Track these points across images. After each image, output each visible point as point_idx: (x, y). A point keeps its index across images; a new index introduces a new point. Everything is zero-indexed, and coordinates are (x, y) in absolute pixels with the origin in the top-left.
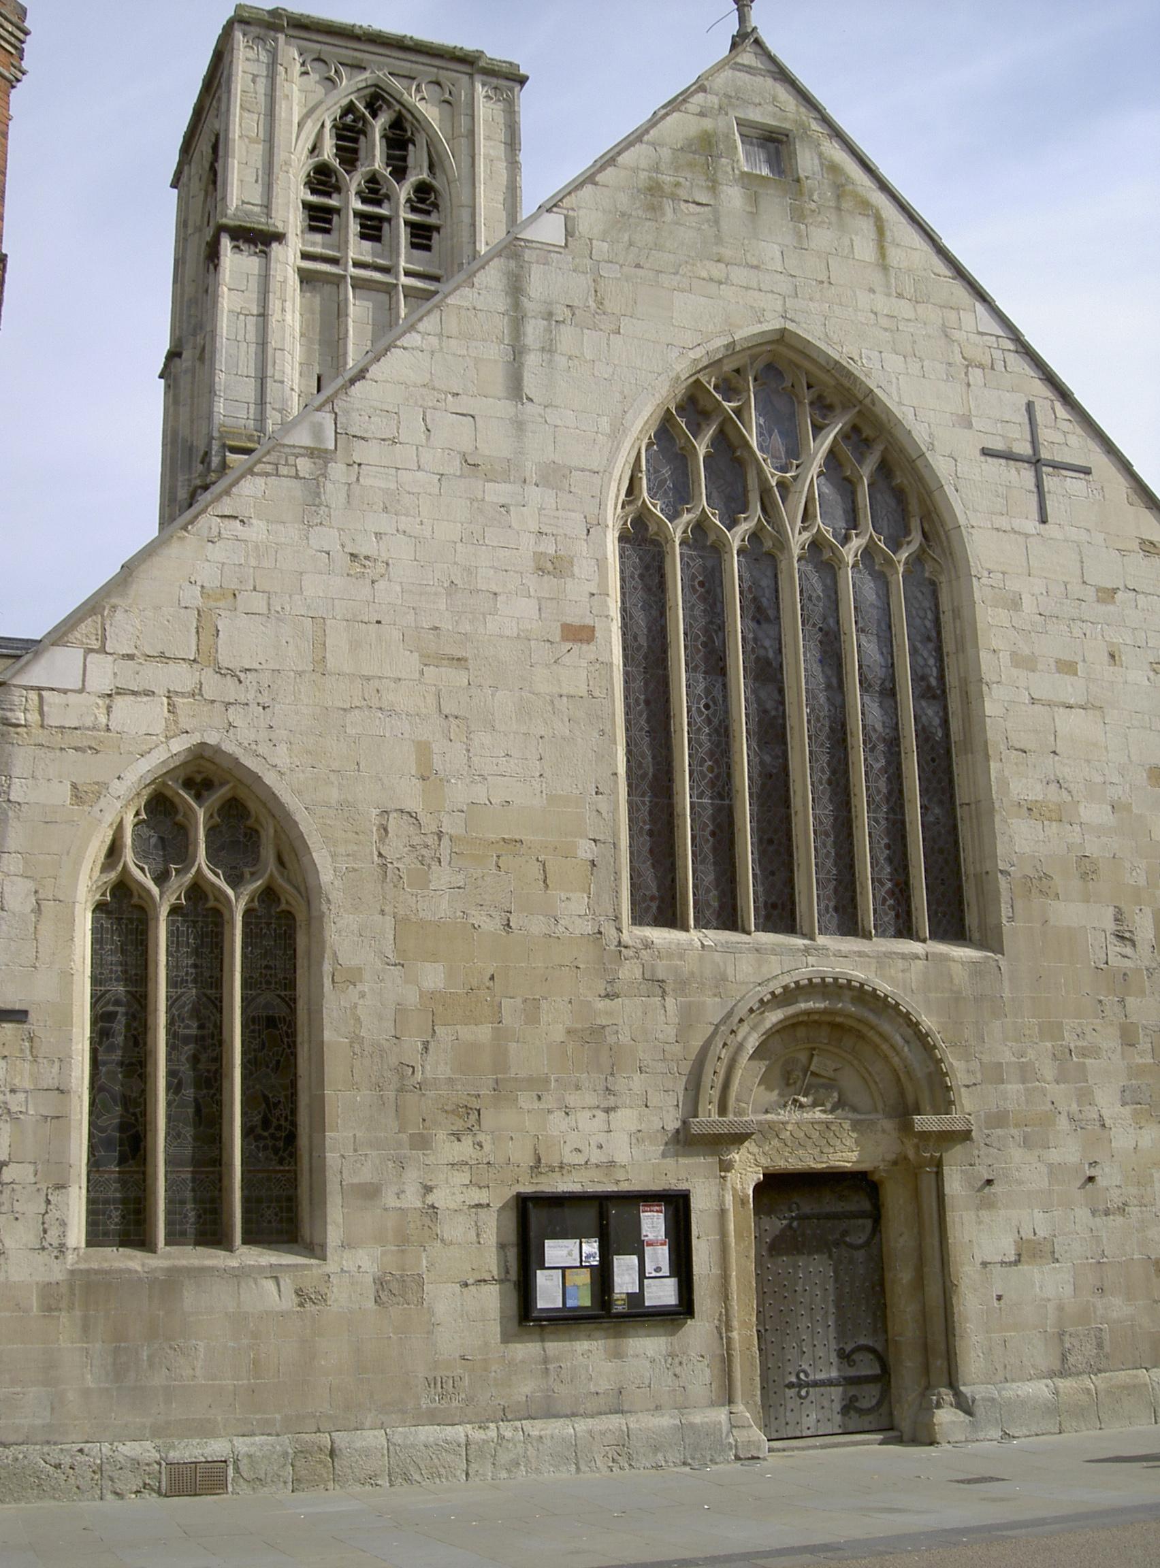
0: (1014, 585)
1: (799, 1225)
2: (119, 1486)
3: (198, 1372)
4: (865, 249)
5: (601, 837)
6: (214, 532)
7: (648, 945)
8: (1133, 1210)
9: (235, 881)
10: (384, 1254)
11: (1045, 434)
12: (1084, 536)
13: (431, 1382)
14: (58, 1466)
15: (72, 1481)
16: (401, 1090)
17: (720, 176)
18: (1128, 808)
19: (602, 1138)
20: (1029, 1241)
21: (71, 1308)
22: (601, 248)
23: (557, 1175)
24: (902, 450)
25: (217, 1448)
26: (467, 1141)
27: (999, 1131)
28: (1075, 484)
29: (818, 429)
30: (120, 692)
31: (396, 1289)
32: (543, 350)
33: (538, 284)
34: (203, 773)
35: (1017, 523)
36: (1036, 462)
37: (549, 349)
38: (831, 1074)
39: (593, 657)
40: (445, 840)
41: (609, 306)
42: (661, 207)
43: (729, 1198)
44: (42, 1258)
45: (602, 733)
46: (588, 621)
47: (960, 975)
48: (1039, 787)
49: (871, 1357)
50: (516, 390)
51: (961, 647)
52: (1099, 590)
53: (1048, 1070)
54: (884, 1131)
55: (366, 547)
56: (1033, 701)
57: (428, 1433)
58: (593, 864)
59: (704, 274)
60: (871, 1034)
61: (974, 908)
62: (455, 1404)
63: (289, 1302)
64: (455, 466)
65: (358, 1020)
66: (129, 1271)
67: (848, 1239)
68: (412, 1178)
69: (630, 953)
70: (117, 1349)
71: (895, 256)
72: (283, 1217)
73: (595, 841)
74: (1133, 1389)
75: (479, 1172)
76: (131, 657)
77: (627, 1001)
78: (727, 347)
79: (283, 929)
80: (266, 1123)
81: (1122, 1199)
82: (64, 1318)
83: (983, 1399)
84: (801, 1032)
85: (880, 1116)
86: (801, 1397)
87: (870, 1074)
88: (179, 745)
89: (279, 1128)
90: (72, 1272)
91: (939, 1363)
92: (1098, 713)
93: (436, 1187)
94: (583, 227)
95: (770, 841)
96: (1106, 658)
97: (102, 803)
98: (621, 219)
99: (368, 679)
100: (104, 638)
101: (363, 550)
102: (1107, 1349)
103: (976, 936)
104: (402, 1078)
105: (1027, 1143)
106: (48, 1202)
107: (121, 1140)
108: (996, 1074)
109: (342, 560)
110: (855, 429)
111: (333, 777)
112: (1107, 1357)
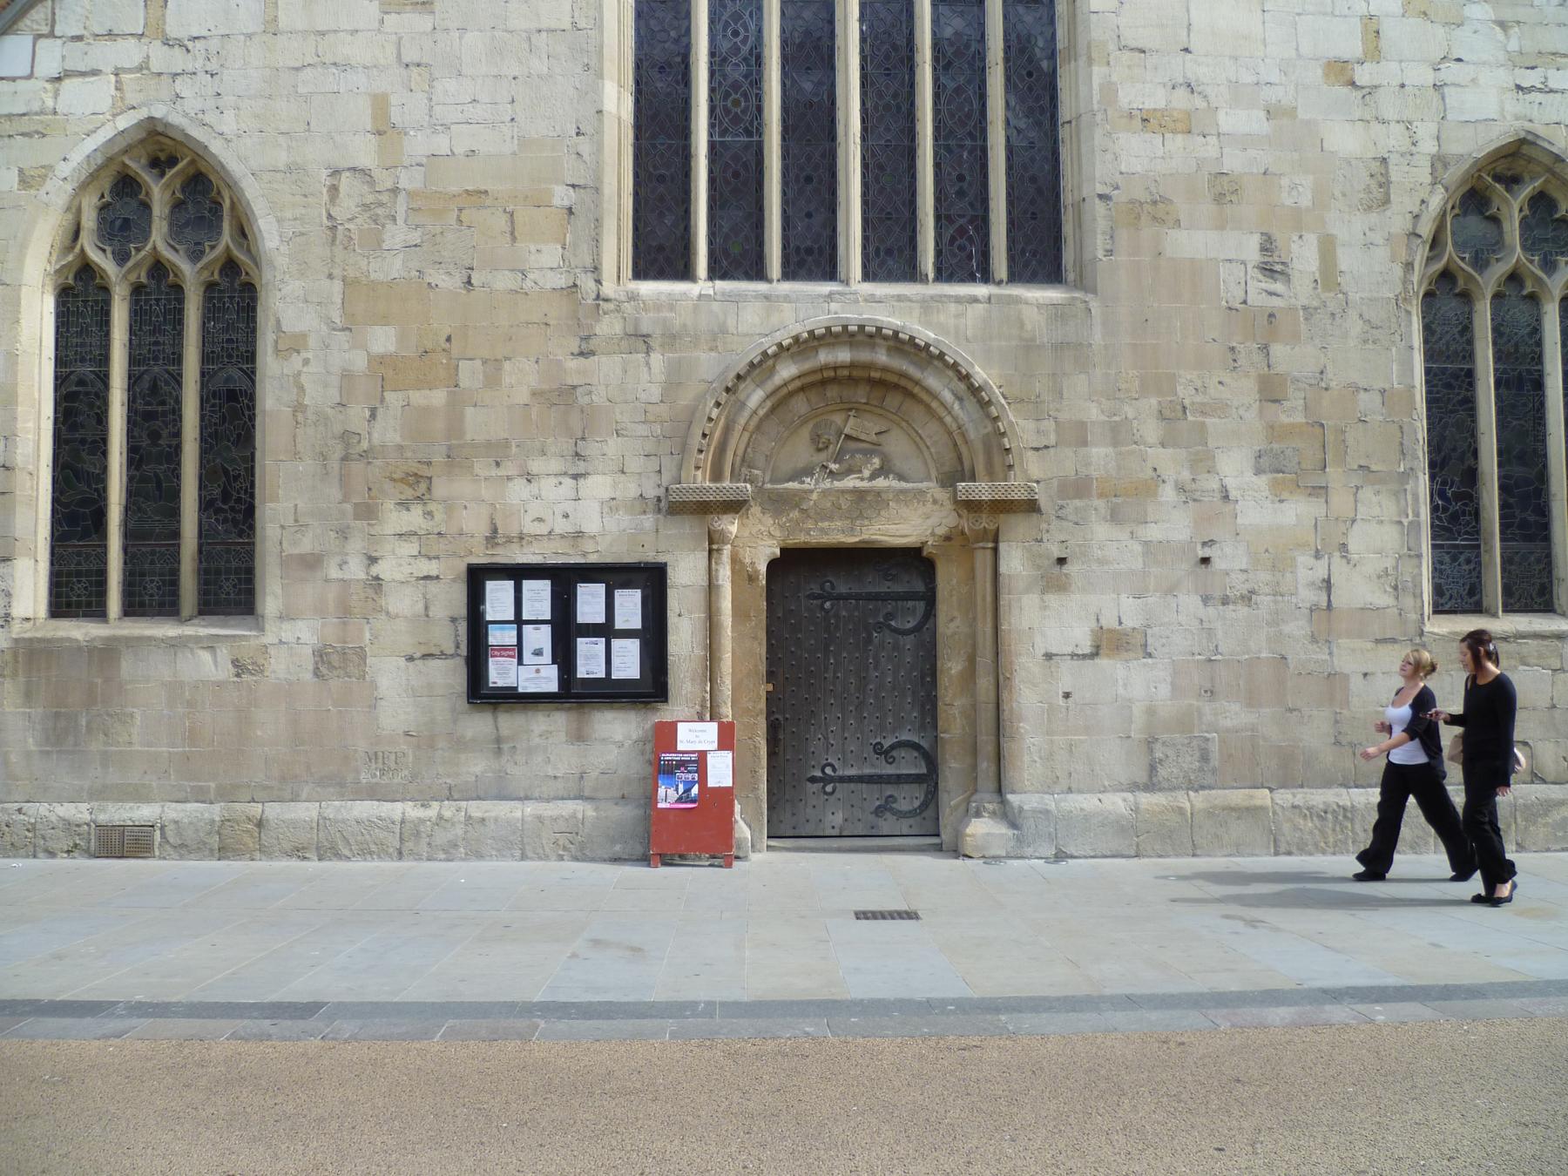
2: (51, 845)
3: (135, 738)
5: (581, 182)
7: (633, 297)
8: (1264, 600)
9: (195, 255)
10: (323, 625)
16: (345, 458)
18: (1291, 112)
19: (568, 507)
20: (1110, 631)
21: (14, 675)
25: (145, 812)
26: (417, 510)
27: (1077, 503)
30: (68, 74)
34: (161, 148)
38: (874, 438)
40: (402, 198)
43: (725, 574)
45: (587, 67)
53: (1151, 430)
54: (935, 502)
57: (364, 809)
58: (570, 211)
60: (916, 390)
62: (397, 780)
63: (225, 672)
65: (301, 389)
66: (69, 639)
68: (356, 546)
69: (611, 306)
70: (57, 715)
72: (231, 590)
73: (573, 186)
74: (1252, 812)
75: (428, 543)
76: (79, 38)
77: (604, 359)
79: (236, 298)
80: (226, 496)
81: (1248, 586)
83: (1034, 811)
84: (832, 392)
89: (239, 500)
90: (16, 640)
93: (382, 557)
95: (809, 179)
97: (49, 185)
99: (323, 34)
100: (54, 21)
103: (1071, 276)
104: (348, 445)
105: (1115, 517)
107: (76, 515)
108: (1079, 435)
111: (281, 139)
112: (1214, 771)
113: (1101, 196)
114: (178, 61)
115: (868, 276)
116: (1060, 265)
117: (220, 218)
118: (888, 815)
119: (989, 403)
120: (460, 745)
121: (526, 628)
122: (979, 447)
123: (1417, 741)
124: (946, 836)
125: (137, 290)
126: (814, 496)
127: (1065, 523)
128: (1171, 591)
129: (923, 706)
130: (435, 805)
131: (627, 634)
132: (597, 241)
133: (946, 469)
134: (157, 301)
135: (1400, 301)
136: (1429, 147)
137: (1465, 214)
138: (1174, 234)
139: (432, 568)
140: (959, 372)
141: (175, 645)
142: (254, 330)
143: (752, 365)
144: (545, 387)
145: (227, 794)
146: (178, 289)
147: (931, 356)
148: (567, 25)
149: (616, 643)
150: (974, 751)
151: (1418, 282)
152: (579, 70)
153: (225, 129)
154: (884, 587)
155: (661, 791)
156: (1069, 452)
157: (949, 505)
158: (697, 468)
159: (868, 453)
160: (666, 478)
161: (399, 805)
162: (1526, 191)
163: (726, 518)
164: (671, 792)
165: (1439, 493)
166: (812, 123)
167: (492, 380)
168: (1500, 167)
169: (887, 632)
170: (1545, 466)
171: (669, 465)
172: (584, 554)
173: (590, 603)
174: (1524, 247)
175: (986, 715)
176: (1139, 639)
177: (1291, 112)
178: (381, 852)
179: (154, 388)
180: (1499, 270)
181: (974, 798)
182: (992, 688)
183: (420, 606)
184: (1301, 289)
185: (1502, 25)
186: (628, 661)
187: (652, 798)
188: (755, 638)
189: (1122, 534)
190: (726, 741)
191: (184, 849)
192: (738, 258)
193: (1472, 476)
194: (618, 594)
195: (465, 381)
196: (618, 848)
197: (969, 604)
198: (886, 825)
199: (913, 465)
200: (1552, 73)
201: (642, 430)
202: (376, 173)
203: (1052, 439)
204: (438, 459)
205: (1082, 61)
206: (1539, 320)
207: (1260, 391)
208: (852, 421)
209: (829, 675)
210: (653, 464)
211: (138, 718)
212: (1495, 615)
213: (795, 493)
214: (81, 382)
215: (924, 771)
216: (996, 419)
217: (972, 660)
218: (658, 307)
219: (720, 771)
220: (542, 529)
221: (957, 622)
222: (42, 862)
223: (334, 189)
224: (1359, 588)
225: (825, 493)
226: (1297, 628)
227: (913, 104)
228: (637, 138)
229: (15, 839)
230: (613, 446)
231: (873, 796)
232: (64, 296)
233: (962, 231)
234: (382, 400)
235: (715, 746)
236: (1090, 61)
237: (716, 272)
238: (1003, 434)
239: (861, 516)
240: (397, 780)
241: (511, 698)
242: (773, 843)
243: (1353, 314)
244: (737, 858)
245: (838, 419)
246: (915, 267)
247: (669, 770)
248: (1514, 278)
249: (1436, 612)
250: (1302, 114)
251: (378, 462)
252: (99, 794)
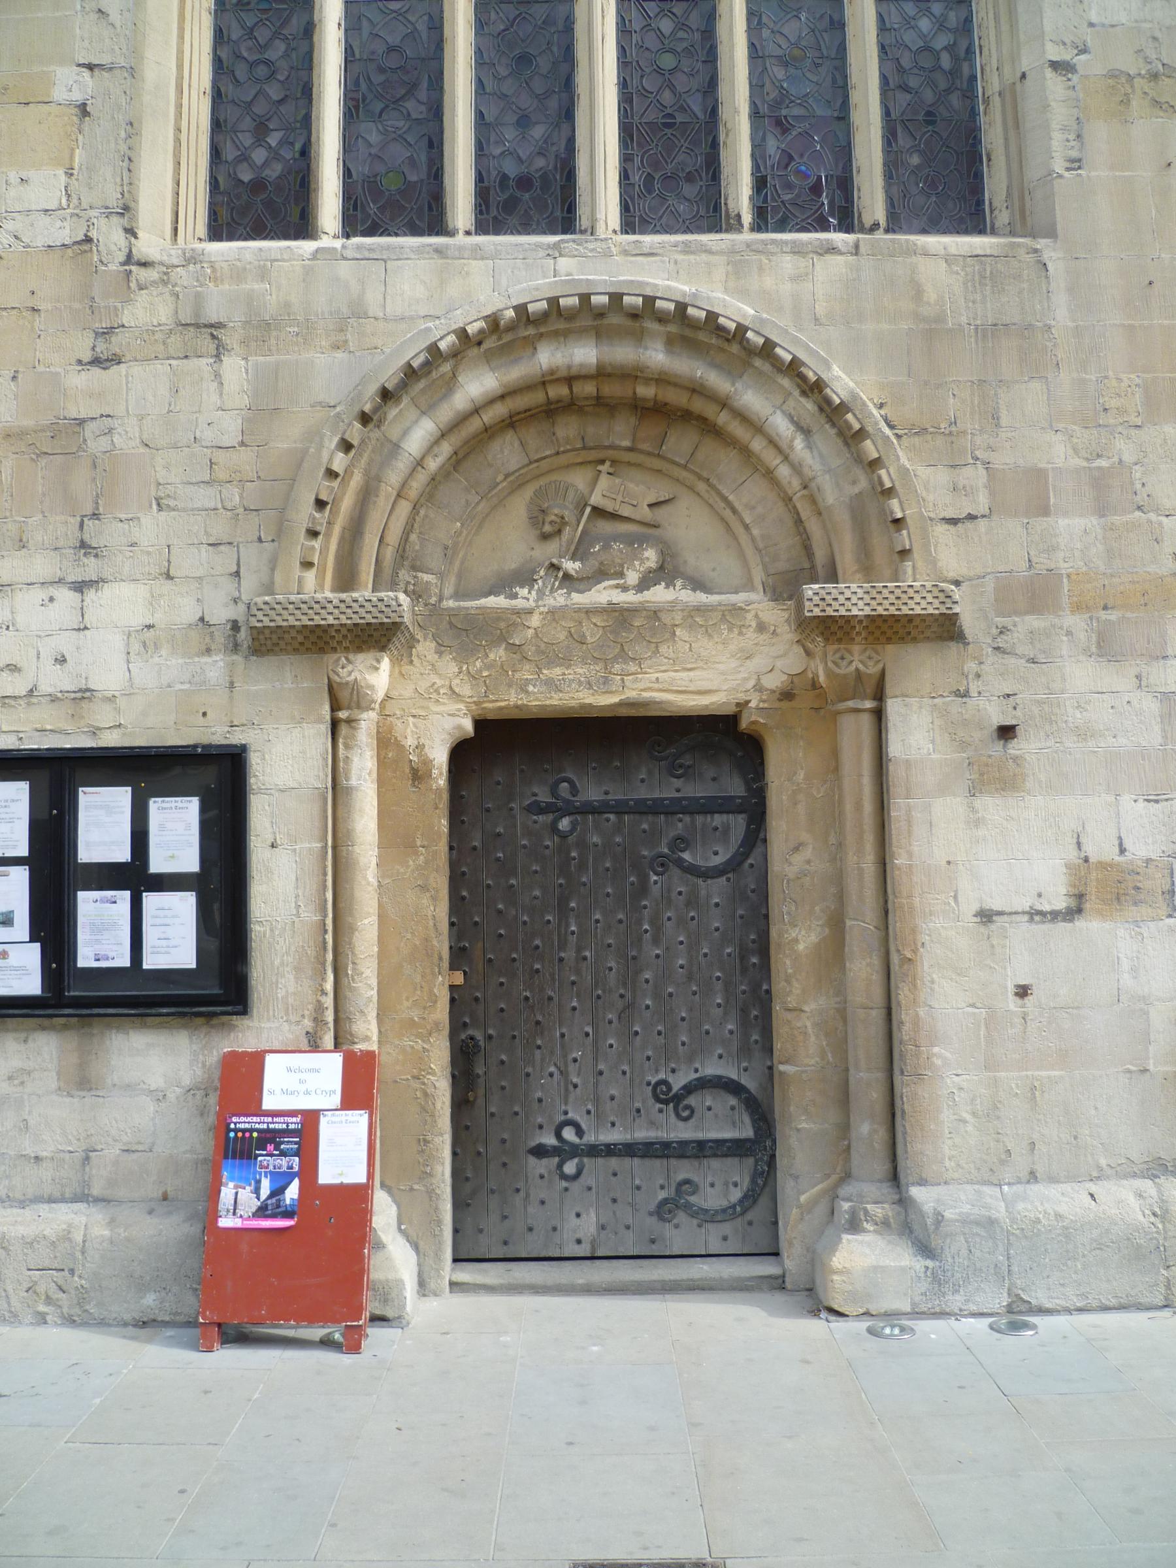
1: (574, 825)
5: (105, 59)
19: (65, 643)
20: (1103, 866)
27: (1034, 622)
38: (645, 513)
43: (363, 767)
49: (733, 1101)
54: (761, 627)
58: (83, 110)
60: (723, 418)
61: (999, 160)
67: (686, 856)
69: (153, 274)
73: (90, 67)
77: (136, 369)
83: (965, 1221)
84: (567, 429)
85: (756, 596)
86: (564, 1177)
87: (734, 511)
103: (1003, 218)
105: (1105, 647)
108: (1034, 496)
113: (1055, 65)
116: (980, 203)
118: (681, 1217)
122: (843, 518)
123: (37, 947)
124: (792, 1262)
126: (535, 621)
127: (1011, 661)
129: (744, 1011)
133: (782, 565)
140: (803, 377)
143: (411, 374)
144: (28, 423)
149: (151, 900)
150: (844, 1098)
154: (669, 789)
155: (227, 1193)
156: (1014, 526)
157: (788, 634)
158: (307, 565)
159: (635, 542)
160: (250, 583)
164: (246, 1194)
169: (675, 871)
171: (253, 558)
172: (94, 732)
181: (844, 1191)
182: (877, 978)
188: (424, 888)
189: (1119, 680)
190: (358, 1090)
192: (396, 201)
196: (150, 1299)
197: (830, 817)
198: (680, 1234)
199: (719, 562)
201: (206, 497)
203: (982, 503)
208: (604, 482)
209: (569, 954)
210: (225, 561)
213: (499, 615)
215: (748, 1132)
216: (875, 464)
217: (837, 924)
221: (807, 853)
225: (554, 614)
230: (150, 529)
231: (655, 1182)
235: (336, 1100)
238: (889, 492)
239: (622, 656)
242: (467, 1274)
244: (379, 1319)
245: (579, 479)
246: (717, 208)
247: (239, 1150)
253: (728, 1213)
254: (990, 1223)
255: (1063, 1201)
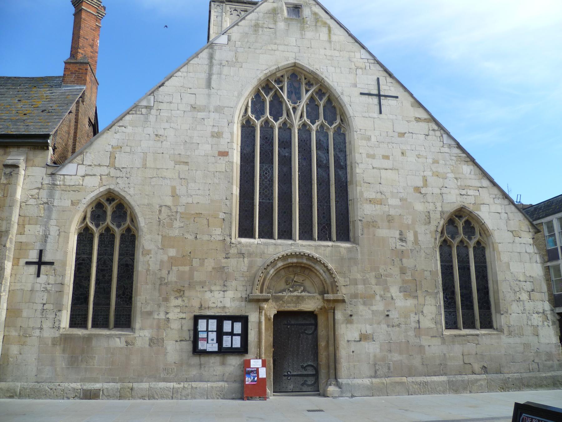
0: (368, 133)
4: (324, 36)
6: (117, 130)
7: (240, 243)
8: (403, 326)
9: (119, 226)
11: (382, 87)
12: (394, 117)
13: (165, 369)
14: (51, 389)
15: (55, 394)
16: (161, 285)
17: (278, 19)
18: (406, 200)
19: (222, 299)
21: (60, 344)
22: (238, 44)
23: (207, 310)
24: (334, 95)
25: (98, 386)
26: (180, 299)
27: (355, 300)
28: (392, 102)
29: (307, 91)
30: (87, 175)
31: (155, 342)
32: (218, 74)
33: (218, 56)
35: (371, 115)
36: (379, 96)
37: (220, 74)
39: (227, 160)
40: (178, 214)
41: (239, 60)
42: (258, 30)
43: (263, 319)
44: (53, 330)
45: (229, 182)
46: (227, 150)
47: (343, 251)
48: (374, 194)
50: (209, 85)
51: (351, 153)
52: (399, 133)
53: (373, 281)
55: (161, 132)
56: (373, 168)
57: (162, 385)
58: (224, 220)
59: (270, 49)
61: (352, 231)
62: (171, 376)
63: (123, 344)
64: (189, 108)
65: (149, 265)
66: (77, 334)
68: (163, 309)
69: (234, 245)
70: (72, 357)
71: (334, 38)
72: (125, 320)
78: (276, 69)
79: (130, 239)
80: (124, 294)
81: (399, 322)
82: (58, 347)
83: (345, 384)
84: (291, 269)
85: (317, 294)
88: (102, 189)
89: (127, 295)
91: (332, 371)
92: (396, 171)
94: (233, 38)
95: (285, 212)
96: (400, 154)
97: (79, 205)
98: (245, 35)
99: (158, 169)
100: (83, 161)
101: (160, 133)
102: (392, 370)
103: (352, 240)
105: (364, 304)
106: (56, 315)
107: (80, 297)
108: (355, 282)
109: (153, 136)
110: (320, 90)
111: (146, 196)
112: (391, 372)
114: (118, 174)
115: (300, 239)
117: (126, 216)
119: (333, 274)
120: (189, 365)
121: (210, 333)
122: (329, 285)
124: (321, 391)
125: (101, 235)
126: (286, 297)
128: (379, 323)
130: (182, 383)
131: (238, 335)
132: (231, 228)
134: (107, 238)
135: (434, 248)
136: (440, 209)
137: (449, 225)
138: (378, 230)
139: (183, 316)
141: (109, 336)
142: (134, 247)
143: (271, 262)
145: (121, 381)
146: (113, 236)
147: (317, 261)
148: (224, 170)
149: (234, 337)
150: (329, 367)
151: (438, 243)
152: (227, 182)
153: (130, 193)
155: (247, 379)
157: (321, 300)
159: (300, 286)
161: (172, 383)
162: (464, 220)
163: (264, 303)
164: (249, 379)
165: (445, 297)
166: (286, 197)
167: (202, 264)
168: (457, 213)
170: (471, 290)
171: (249, 289)
173: (227, 326)
174: (464, 234)
175: (332, 357)
176: (371, 337)
177: (406, 200)
178: (167, 397)
179: (105, 263)
180: (458, 240)
183: (180, 326)
184: (410, 245)
185: (456, 178)
186: (237, 342)
187: (244, 381)
190: (264, 365)
191: (109, 397)
192: (266, 233)
193: (453, 293)
194: (235, 323)
195: (194, 264)
196: (234, 395)
197: (327, 327)
198: (305, 388)
200: (468, 191)
201: (242, 279)
202: (172, 207)
204: (186, 285)
205: (354, 185)
206: (468, 252)
207: (400, 271)
211: (97, 357)
212: (461, 329)
213: (281, 296)
214: (83, 260)
215: (314, 373)
216: (334, 278)
218: (246, 246)
219: (263, 373)
220: (214, 305)
222: (66, 401)
223: (160, 211)
224: (427, 323)
225: (289, 296)
226: (411, 333)
227: (312, 194)
228: (240, 199)
229: (57, 394)
230: (234, 283)
231: (301, 380)
232: (80, 236)
233: (324, 227)
234: (171, 269)
236: (357, 186)
237: (261, 236)
239: (298, 303)
240: (171, 376)
241: (205, 353)
242: (275, 394)
243: (422, 251)
247: (249, 373)
248: (462, 242)
249: (446, 329)
250: (409, 200)
251: (170, 286)
252: (83, 380)
253: (312, 385)
254: (349, 384)
255: (359, 381)
